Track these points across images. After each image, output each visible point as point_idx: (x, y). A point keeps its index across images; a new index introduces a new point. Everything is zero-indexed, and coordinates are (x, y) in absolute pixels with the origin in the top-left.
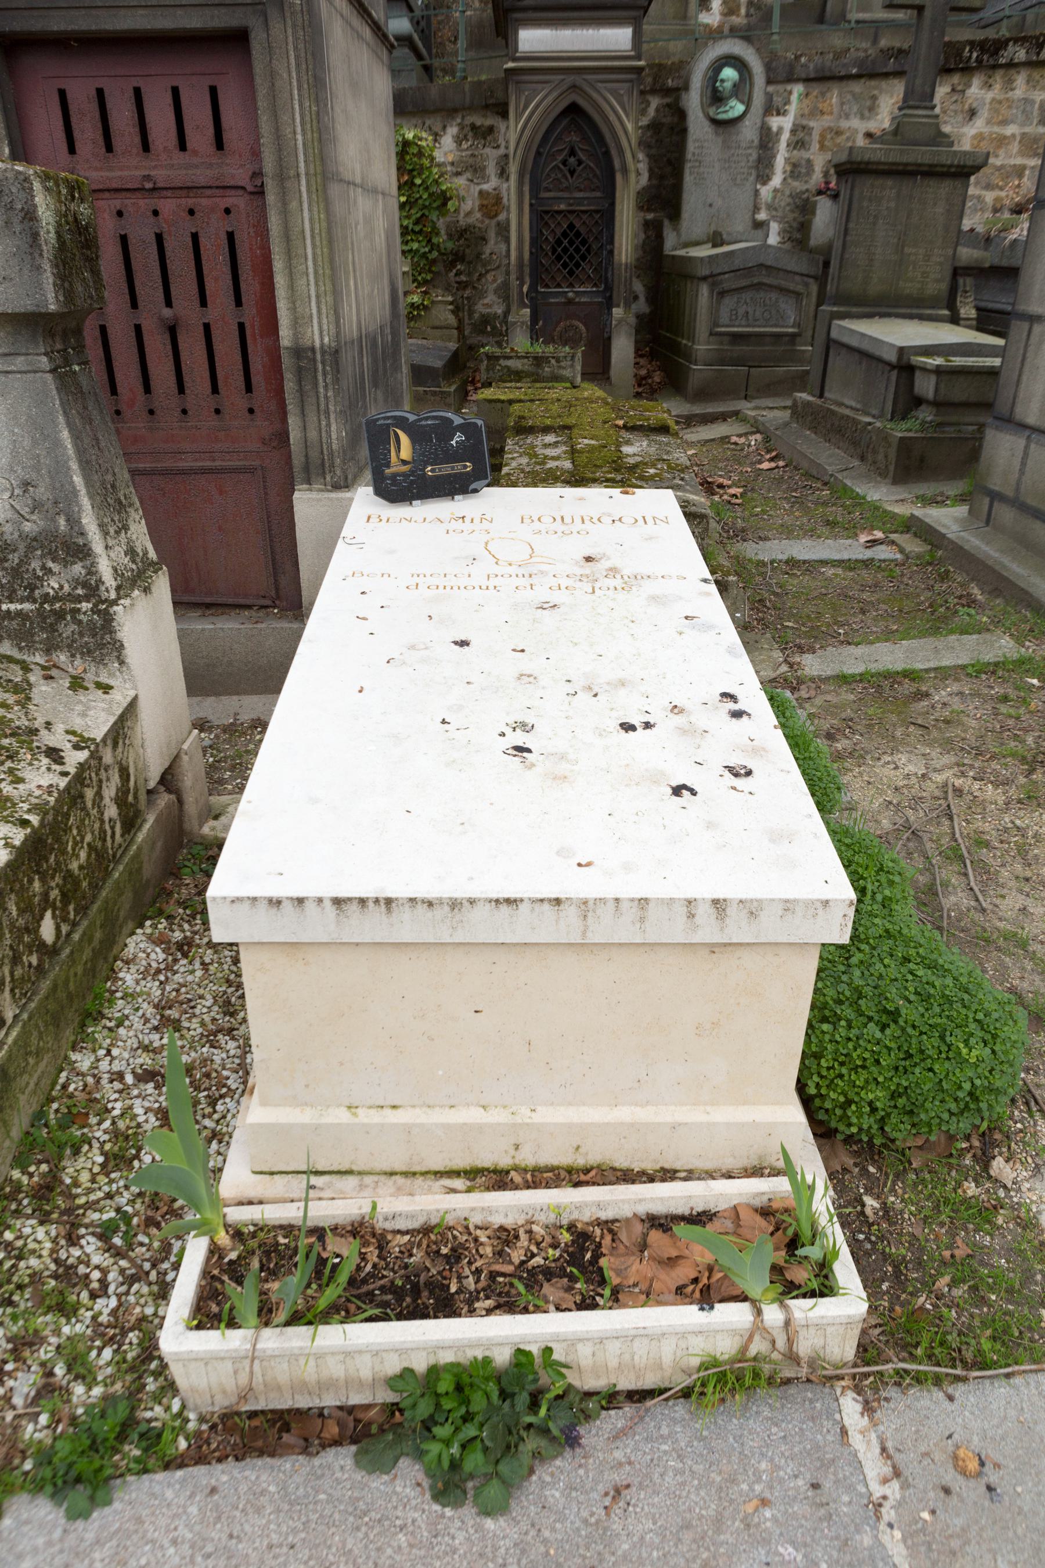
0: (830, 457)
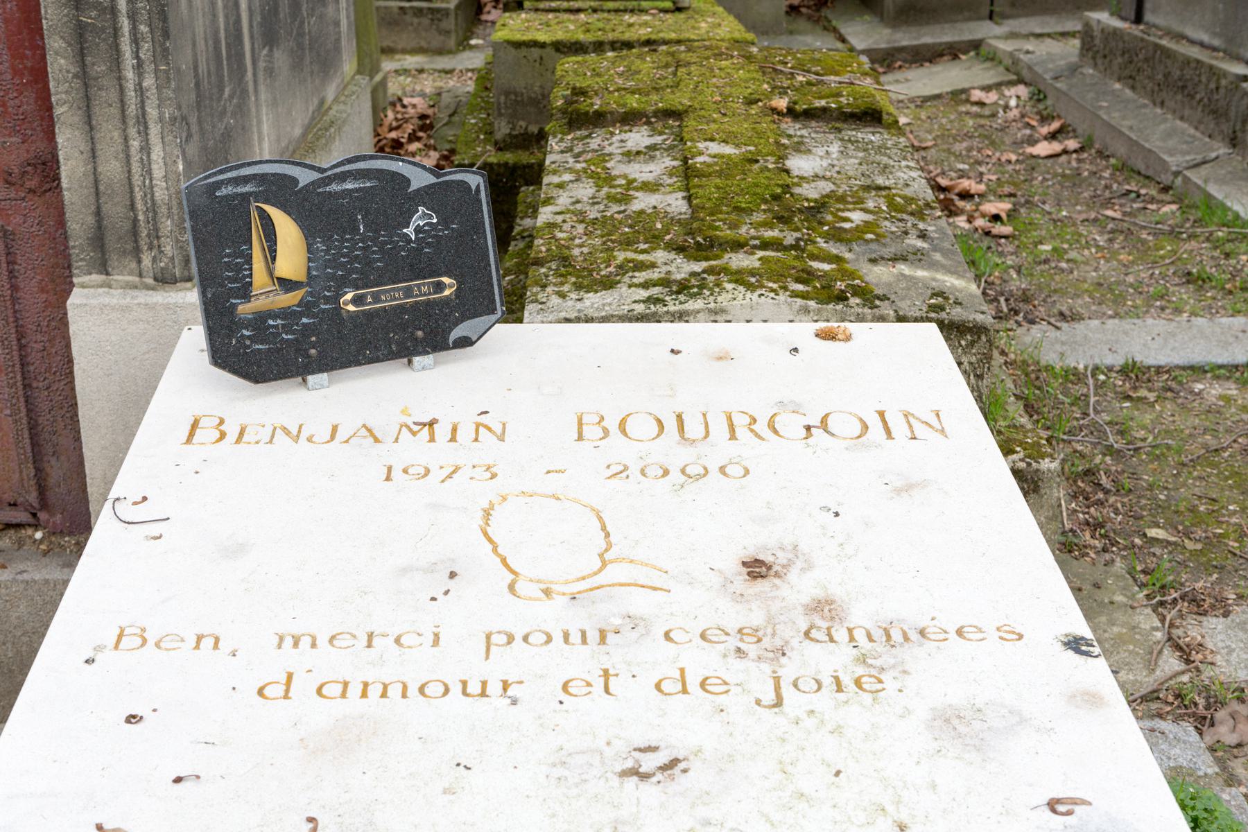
0: (1169, 137)
